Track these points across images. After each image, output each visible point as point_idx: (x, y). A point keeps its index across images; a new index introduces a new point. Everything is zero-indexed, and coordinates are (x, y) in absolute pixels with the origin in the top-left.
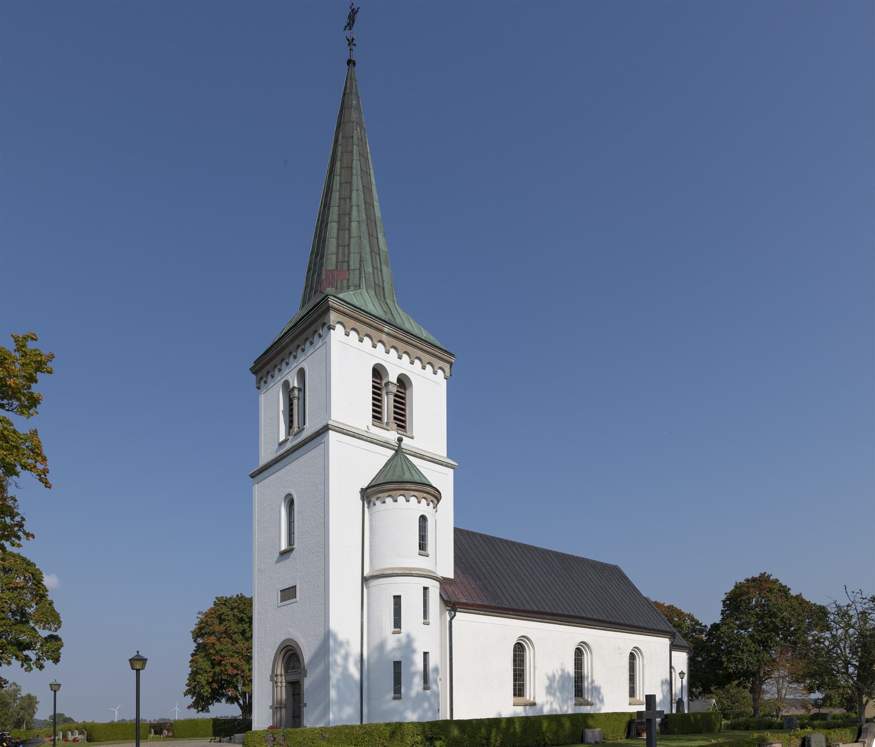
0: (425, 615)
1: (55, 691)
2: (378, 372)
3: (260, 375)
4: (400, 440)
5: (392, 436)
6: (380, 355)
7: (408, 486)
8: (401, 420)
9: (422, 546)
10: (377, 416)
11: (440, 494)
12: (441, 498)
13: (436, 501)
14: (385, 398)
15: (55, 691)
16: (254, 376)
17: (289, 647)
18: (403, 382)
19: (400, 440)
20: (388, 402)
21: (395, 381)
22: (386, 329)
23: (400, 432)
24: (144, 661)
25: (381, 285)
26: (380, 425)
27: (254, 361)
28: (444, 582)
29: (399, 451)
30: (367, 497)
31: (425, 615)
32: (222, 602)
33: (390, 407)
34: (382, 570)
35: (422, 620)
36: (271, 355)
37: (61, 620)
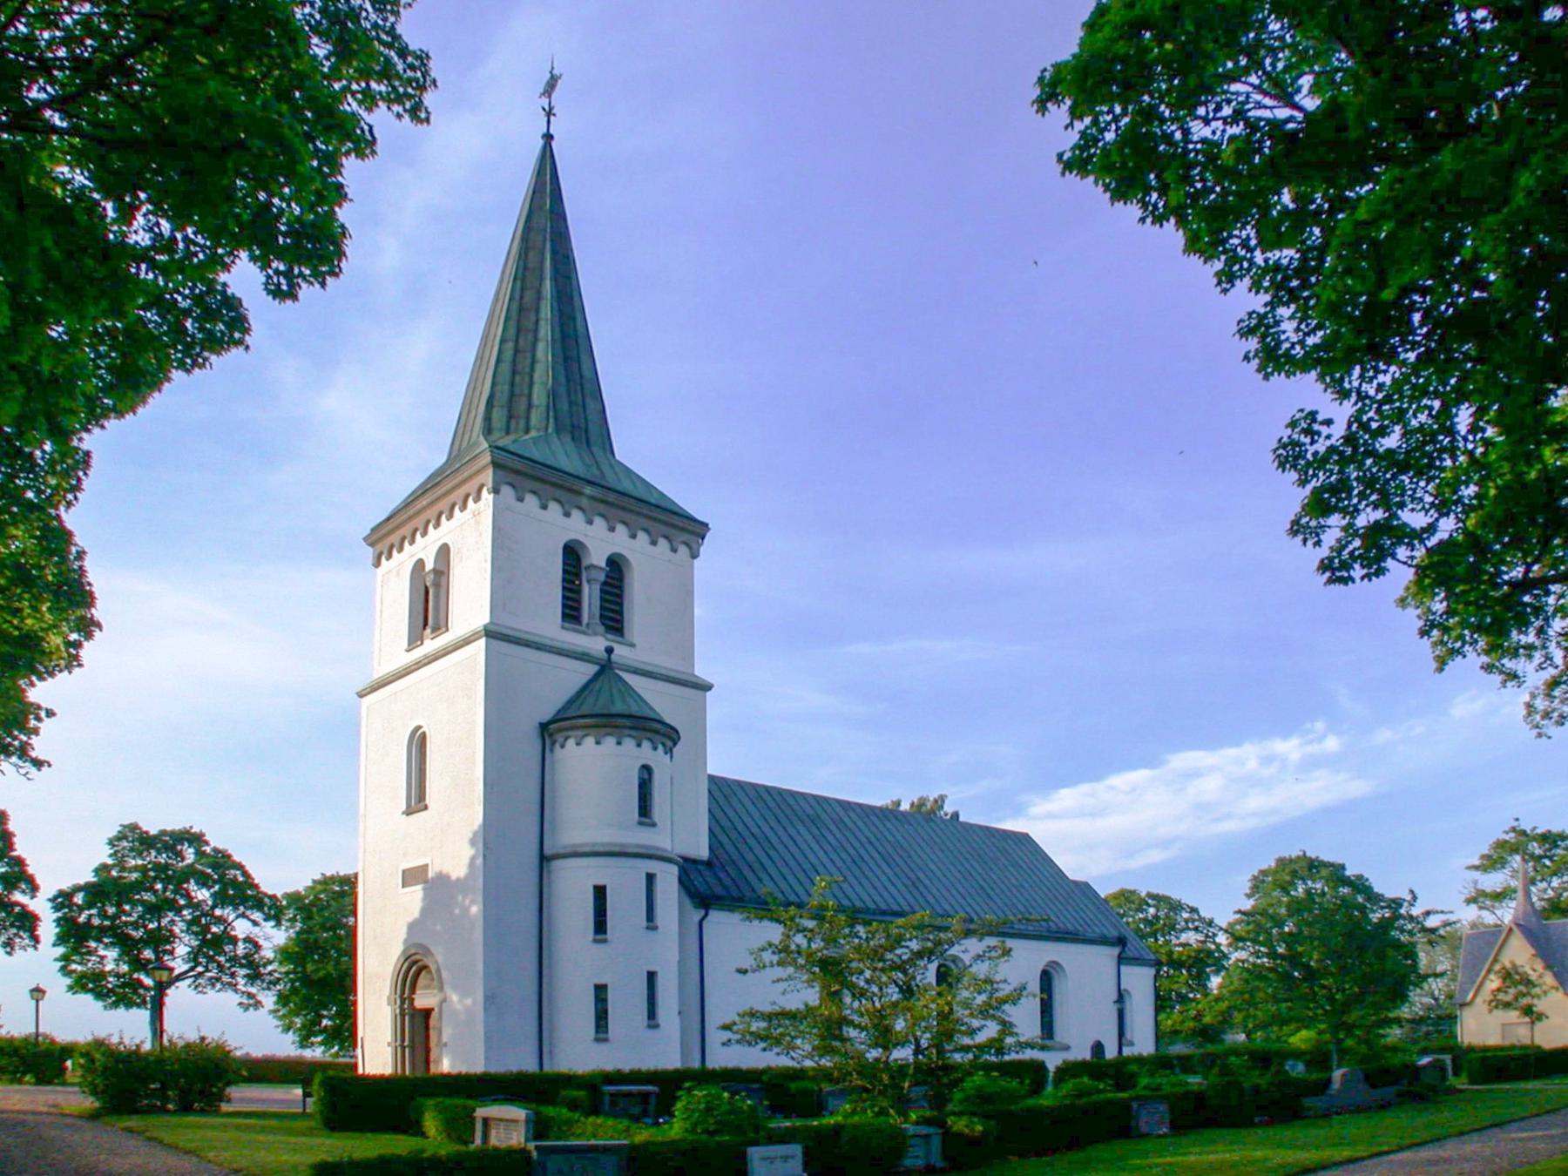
0: (652, 1014)
1: (37, 1001)
2: (573, 554)
3: (379, 547)
4: (610, 651)
5: (596, 644)
6: (576, 527)
7: (620, 721)
8: (613, 621)
9: (645, 808)
10: (571, 612)
11: (677, 732)
12: (679, 738)
13: (669, 744)
14: (586, 588)
15: (37, 1001)
16: (370, 549)
17: (414, 958)
18: (616, 566)
19: (610, 651)
20: (590, 596)
21: (603, 564)
22: (588, 490)
23: (609, 636)
24: (44, 992)
25: (583, 426)
26: (577, 627)
27: (373, 525)
28: (687, 866)
29: (606, 667)
30: (551, 735)
31: (652, 1014)
32: (326, 881)
33: (593, 601)
34: (574, 845)
35: (644, 923)
36: (395, 522)
37: (256, 881)
